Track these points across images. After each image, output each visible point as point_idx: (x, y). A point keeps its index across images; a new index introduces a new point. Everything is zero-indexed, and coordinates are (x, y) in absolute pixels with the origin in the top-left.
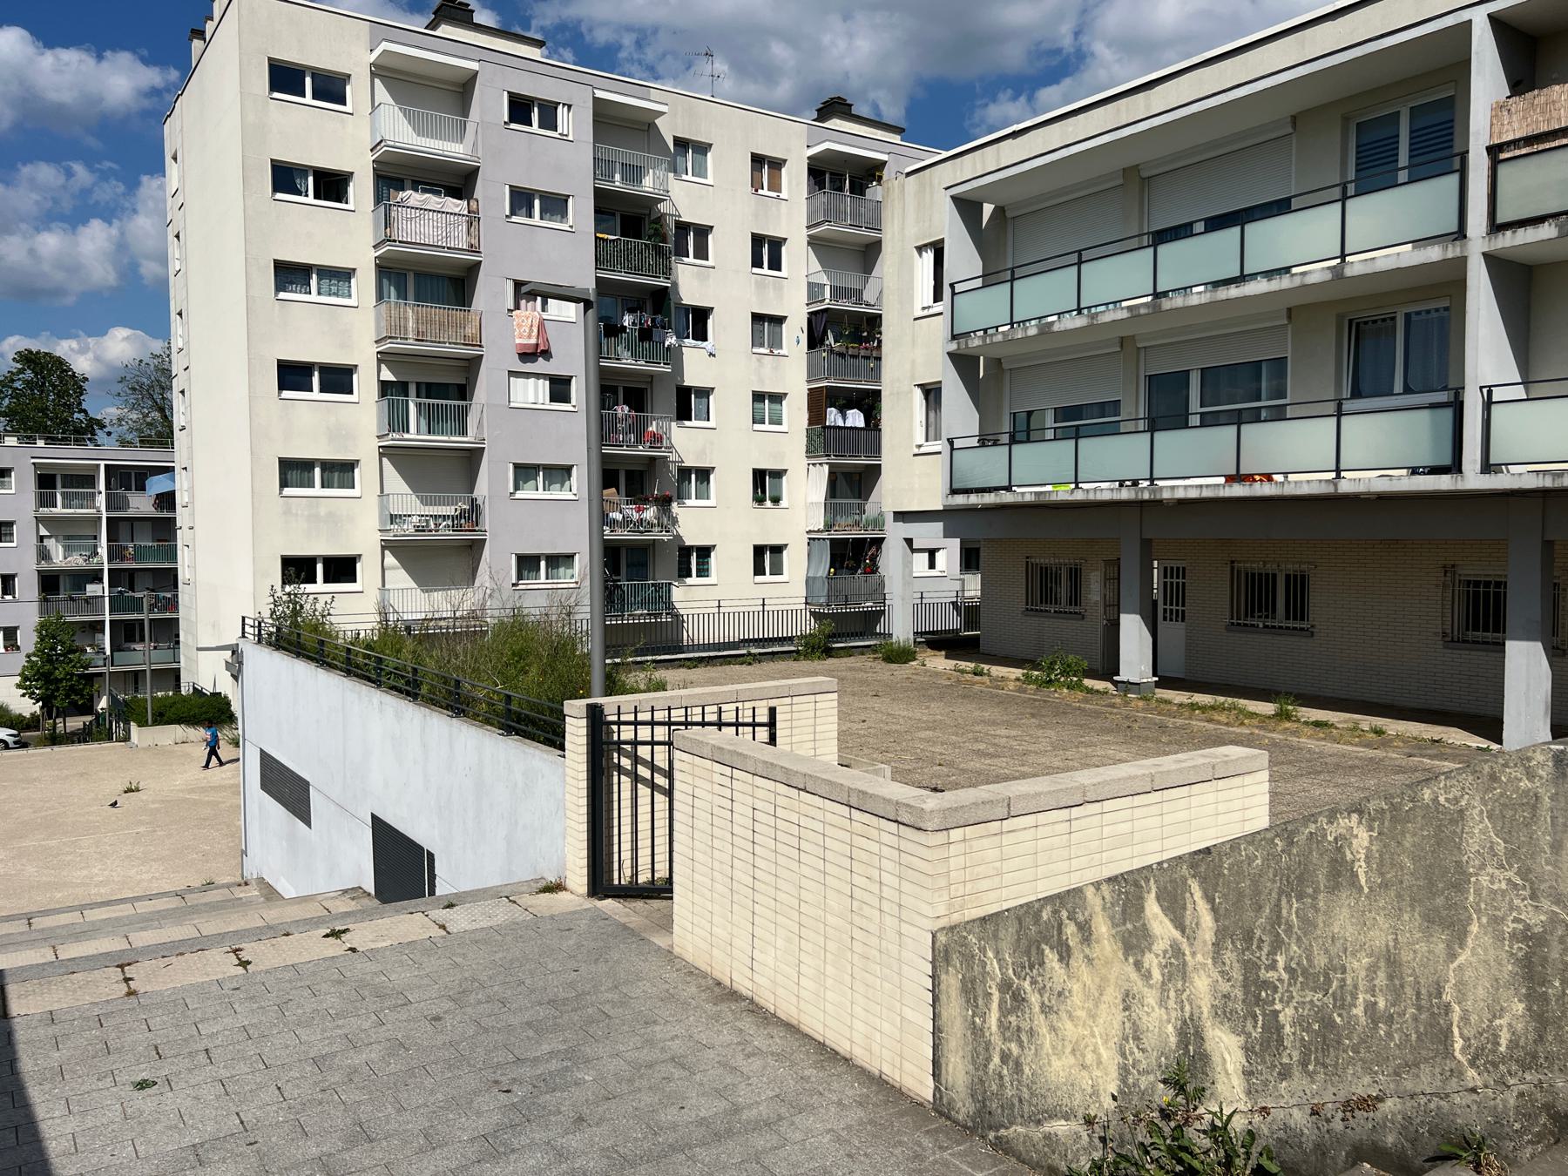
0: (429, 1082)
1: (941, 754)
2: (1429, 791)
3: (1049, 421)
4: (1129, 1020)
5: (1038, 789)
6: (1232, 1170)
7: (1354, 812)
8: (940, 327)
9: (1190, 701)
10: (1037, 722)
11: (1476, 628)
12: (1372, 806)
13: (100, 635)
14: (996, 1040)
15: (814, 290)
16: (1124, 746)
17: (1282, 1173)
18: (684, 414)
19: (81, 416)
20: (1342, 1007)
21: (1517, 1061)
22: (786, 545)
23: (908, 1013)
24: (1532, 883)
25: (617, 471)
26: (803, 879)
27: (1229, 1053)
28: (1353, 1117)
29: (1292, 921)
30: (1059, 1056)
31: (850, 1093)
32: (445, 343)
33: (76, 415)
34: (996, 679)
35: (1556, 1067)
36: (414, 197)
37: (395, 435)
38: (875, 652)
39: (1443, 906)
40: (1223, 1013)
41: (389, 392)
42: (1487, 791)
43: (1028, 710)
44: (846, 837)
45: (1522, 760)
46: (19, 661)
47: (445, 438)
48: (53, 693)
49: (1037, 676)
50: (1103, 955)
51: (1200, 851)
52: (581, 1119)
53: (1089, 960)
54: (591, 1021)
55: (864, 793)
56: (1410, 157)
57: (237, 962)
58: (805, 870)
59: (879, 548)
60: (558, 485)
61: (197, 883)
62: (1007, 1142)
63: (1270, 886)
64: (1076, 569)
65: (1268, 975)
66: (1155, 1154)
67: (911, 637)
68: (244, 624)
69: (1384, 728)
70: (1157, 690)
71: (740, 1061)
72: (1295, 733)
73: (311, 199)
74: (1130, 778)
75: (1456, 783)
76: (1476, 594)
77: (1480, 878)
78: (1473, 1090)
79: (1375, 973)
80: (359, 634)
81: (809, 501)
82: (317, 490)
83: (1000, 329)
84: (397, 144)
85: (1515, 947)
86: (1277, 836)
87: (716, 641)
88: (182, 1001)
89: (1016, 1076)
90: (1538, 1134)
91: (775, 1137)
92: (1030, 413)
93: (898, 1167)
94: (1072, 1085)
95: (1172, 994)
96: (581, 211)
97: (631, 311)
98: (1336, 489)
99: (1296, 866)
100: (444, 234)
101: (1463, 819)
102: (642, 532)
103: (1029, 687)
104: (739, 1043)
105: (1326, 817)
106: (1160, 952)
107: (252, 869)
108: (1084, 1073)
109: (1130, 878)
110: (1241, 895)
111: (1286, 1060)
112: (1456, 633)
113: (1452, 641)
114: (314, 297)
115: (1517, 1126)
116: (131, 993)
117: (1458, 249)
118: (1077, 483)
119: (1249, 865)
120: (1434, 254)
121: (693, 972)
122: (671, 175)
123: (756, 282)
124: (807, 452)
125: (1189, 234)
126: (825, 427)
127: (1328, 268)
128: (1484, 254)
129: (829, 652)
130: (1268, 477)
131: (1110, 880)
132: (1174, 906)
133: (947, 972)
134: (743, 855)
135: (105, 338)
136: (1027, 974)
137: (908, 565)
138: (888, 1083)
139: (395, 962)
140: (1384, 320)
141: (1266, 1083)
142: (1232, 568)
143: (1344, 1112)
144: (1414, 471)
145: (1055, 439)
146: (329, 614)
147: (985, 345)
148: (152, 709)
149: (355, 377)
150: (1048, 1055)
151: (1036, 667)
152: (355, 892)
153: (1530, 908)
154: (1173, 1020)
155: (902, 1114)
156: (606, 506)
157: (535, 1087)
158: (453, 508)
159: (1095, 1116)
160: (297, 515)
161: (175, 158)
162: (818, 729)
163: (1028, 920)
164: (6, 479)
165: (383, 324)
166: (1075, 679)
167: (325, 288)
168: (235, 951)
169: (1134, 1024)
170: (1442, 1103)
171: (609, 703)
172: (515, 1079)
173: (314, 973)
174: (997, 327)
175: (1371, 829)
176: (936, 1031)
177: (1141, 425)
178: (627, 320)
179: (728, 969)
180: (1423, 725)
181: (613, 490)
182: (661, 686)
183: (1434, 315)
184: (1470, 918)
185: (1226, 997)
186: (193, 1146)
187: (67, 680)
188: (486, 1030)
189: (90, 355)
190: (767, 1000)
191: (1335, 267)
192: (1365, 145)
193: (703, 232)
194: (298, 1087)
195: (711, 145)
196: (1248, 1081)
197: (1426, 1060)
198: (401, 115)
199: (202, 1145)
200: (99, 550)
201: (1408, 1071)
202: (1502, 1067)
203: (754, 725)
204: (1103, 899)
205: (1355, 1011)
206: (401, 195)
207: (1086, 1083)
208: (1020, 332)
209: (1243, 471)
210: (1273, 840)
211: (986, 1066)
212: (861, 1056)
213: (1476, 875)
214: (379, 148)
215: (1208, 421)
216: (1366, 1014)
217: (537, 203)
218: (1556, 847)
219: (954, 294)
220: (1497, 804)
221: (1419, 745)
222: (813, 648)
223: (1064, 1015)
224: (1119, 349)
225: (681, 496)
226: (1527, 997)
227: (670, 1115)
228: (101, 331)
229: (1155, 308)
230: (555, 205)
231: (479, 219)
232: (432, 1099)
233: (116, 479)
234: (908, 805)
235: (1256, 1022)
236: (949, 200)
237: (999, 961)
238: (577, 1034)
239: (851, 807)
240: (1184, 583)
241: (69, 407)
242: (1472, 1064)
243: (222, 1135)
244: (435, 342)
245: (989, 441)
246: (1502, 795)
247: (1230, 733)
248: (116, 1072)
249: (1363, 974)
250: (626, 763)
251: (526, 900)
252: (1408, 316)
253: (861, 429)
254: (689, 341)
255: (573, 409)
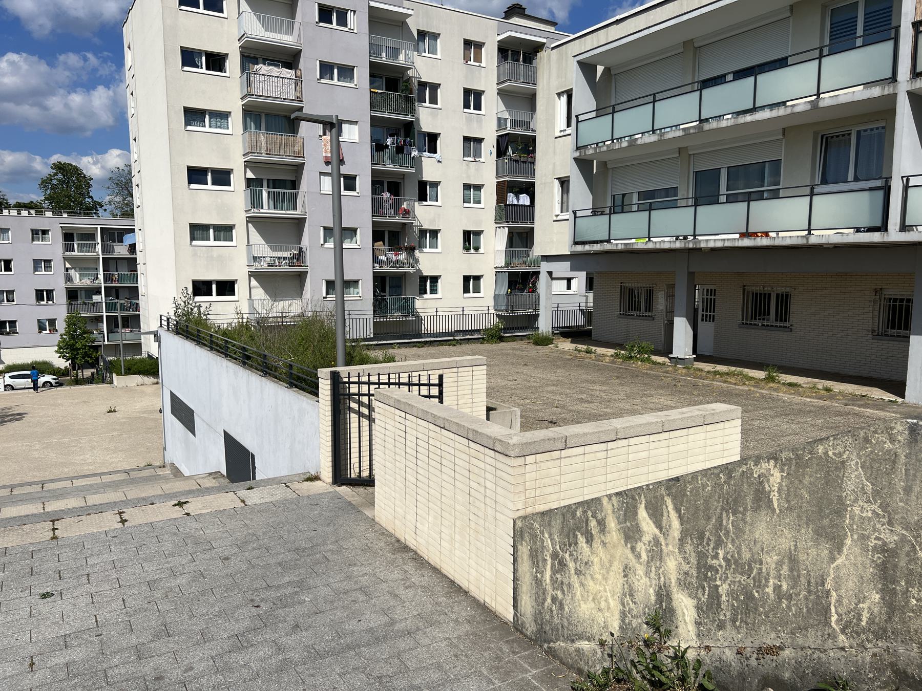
0: (212, 599)
1: (558, 400)
2: (822, 447)
3: (635, 199)
4: (627, 583)
5: (586, 431)
6: (685, 684)
7: (771, 459)
8: (570, 142)
9: (714, 370)
10: (619, 382)
11: (893, 328)
12: (784, 455)
13: (101, 324)
14: (549, 588)
15: (501, 122)
16: (670, 397)
17: (717, 689)
18: (422, 197)
19: (90, 200)
20: (759, 586)
21: (873, 633)
22: (482, 276)
23: (500, 568)
24: (889, 514)
25: (383, 232)
26: (443, 482)
27: (687, 610)
28: (764, 658)
29: (729, 528)
30: (585, 601)
31: (464, 614)
32: (283, 155)
33: (87, 199)
34: (600, 356)
35: (899, 639)
36: (264, 69)
37: (256, 210)
38: (529, 339)
39: (828, 525)
40: (684, 583)
41: (252, 184)
42: (861, 450)
43: (615, 374)
44: (466, 457)
45: (887, 429)
46: (56, 338)
47: (284, 212)
48: (75, 356)
49: (623, 354)
50: (612, 541)
51: (672, 479)
52: (297, 626)
53: (604, 544)
54: (317, 563)
55: (477, 432)
56: (864, 31)
57: (120, 520)
58: (445, 477)
59: (537, 277)
60: (349, 240)
61: (142, 465)
62: (555, 651)
63: (716, 505)
64: (650, 290)
65: (713, 562)
66: (641, 668)
67: (550, 330)
68: (161, 320)
69: (832, 387)
70: (695, 363)
71: (401, 591)
72: (776, 390)
73: (204, 70)
74: (648, 424)
75: (840, 443)
76: (894, 306)
77: (854, 508)
78: (843, 649)
79: (781, 566)
80: (219, 326)
81: (496, 249)
82: (212, 242)
83: (607, 143)
84: (253, 36)
85: (876, 556)
86: (721, 472)
87: (441, 331)
88: (82, 543)
89: (560, 612)
90: (884, 682)
91: (413, 642)
92: (624, 195)
93: (485, 664)
94: (593, 620)
95: (653, 569)
96: (362, 76)
97: (391, 135)
98: (808, 241)
99: (733, 493)
100: (281, 90)
101: (844, 467)
102: (397, 268)
103: (618, 360)
104: (402, 580)
105: (754, 461)
106: (647, 542)
107: (168, 460)
108: (600, 614)
109: (629, 494)
110: (697, 508)
111: (722, 617)
112: (880, 330)
113: (878, 335)
114: (207, 129)
115: (871, 675)
116: (54, 538)
117: (891, 89)
118: (649, 238)
119: (703, 490)
120: (876, 92)
121: (385, 533)
122: (415, 53)
123: (466, 117)
124: (495, 220)
125: (723, 82)
126: (506, 205)
127: (809, 102)
128: (907, 92)
129: (501, 339)
130: (766, 234)
131: (617, 494)
132: (656, 514)
133: (522, 545)
134: (411, 465)
135: (107, 155)
136: (567, 549)
137: (549, 287)
138: (488, 609)
139: (211, 522)
140: (843, 135)
141: (709, 630)
142: (744, 290)
143: (757, 654)
144: (858, 230)
145: (638, 211)
146: (208, 314)
147: (596, 153)
148: (124, 366)
149: (232, 176)
150: (578, 600)
151: (623, 348)
152: (215, 475)
153: (887, 531)
154: (653, 586)
155: (494, 629)
156: (377, 252)
157: (274, 604)
158: (289, 253)
159: (606, 641)
160: (200, 256)
161: (129, 48)
162: (474, 387)
163: (569, 516)
164: (46, 236)
165: (247, 145)
166: (646, 356)
167: (213, 124)
168: (120, 513)
169: (630, 586)
170: (822, 655)
171: (343, 370)
172: (263, 599)
173: (162, 528)
174: (604, 142)
175: (782, 471)
176: (515, 580)
177: (690, 202)
178: (389, 141)
179: (403, 532)
180: (857, 386)
181: (381, 243)
182: (392, 359)
183: (876, 131)
184: (846, 534)
185: (686, 573)
186: (65, 635)
187: (83, 349)
188: (254, 567)
189: (99, 165)
190: (424, 553)
191: (813, 101)
192: (835, 23)
193: (435, 87)
194: (135, 599)
195: (439, 34)
196: (698, 628)
197: (812, 626)
198: (255, 18)
199: (70, 635)
200: (99, 276)
201: (800, 632)
202: (862, 635)
203: (420, 385)
204: (613, 505)
205: (767, 590)
206: (256, 67)
207: (601, 620)
208: (617, 145)
209: (750, 231)
210: (719, 474)
211: (543, 604)
212: (474, 591)
213: (852, 506)
214: (243, 38)
215: (731, 199)
216: (774, 592)
217: (336, 71)
218: (908, 490)
219: (578, 122)
220: (868, 458)
221: (853, 399)
222: (492, 336)
223: (589, 577)
224: (678, 155)
225: (421, 246)
226: (883, 591)
227: (351, 625)
228: (103, 151)
229: (699, 128)
230: (346, 72)
231: (302, 81)
232: (211, 610)
233: (107, 236)
234: (500, 441)
235: (704, 591)
236: (576, 64)
237: (551, 540)
238: (307, 571)
239: (469, 440)
240: (714, 299)
241: (82, 194)
242: (843, 631)
243: (83, 629)
244: (277, 155)
245: (598, 212)
246: (872, 452)
247: (736, 389)
248: (32, 587)
249: (773, 566)
250: (354, 405)
251: (296, 486)
252: (859, 132)
253: (528, 206)
254: (426, 154)
255: (357, 195)
